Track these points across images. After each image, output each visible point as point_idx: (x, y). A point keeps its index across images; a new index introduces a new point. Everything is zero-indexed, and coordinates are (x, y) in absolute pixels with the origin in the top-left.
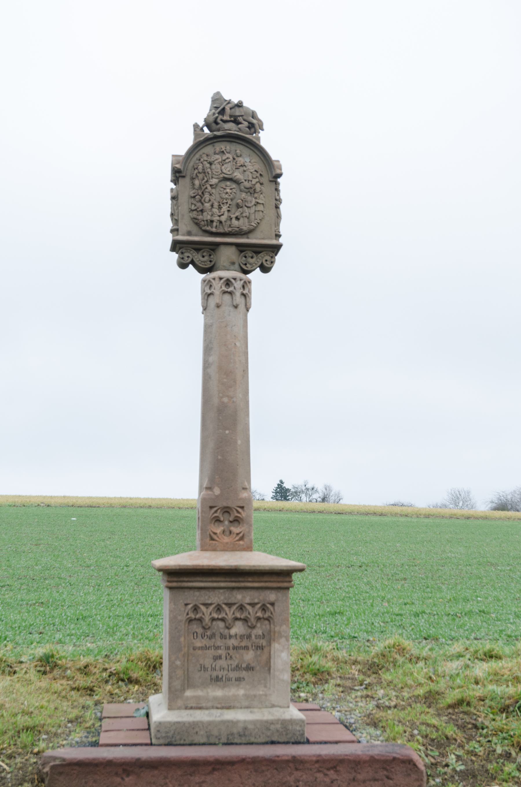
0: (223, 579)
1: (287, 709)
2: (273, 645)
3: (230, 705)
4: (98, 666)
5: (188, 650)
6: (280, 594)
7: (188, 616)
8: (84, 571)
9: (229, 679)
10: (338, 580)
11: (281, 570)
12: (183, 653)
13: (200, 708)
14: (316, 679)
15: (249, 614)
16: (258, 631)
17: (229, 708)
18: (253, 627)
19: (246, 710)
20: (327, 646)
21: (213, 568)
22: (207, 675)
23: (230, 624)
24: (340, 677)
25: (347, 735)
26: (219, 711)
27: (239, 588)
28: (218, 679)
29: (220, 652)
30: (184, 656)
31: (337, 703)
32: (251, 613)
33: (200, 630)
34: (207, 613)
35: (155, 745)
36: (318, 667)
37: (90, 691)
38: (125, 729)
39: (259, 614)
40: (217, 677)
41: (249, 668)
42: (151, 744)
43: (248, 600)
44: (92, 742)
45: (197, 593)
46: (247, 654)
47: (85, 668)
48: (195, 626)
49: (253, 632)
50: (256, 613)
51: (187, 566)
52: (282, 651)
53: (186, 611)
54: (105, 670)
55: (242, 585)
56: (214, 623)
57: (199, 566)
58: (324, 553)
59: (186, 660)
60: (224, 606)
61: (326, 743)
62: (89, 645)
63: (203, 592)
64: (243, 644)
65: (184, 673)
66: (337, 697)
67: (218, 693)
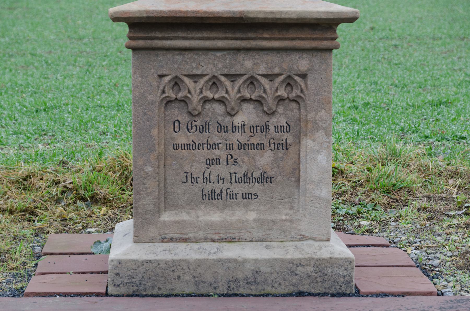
0: (221, 35)
1: (327, 243)
2: (303, 142)
3: (233, 236)
4: (45, 178)
5: (166, 149)
6: (316, 60)
7: (164, 95)
8: (72, 46)
9: (232, 196)
10: (460, 58)
11: (317, 19)
12: (156, 153)
13: (185, 240)
14: (390, 200)
15: (265, 92)
16: (280, 120)
17: (232, 240)
18: (272, 113)
19: (259, 243)
20: (411, 150)
21: (203, 15)
22: (196, 188)
23: (233, 109)
24: (428, 197)
25: (425, 284)
26: (217, 245)
27: (248, 50)
28: (214, 195)
29: (217, 152)
30: (158, 158)
31: (416, 237)
32: (269, 91)
33: (184, 118)
34: (194, 90)
35: (111, 295)
36: (393, 181)
37: (31, 214)
38: (71, 272)
39: (282, 92)
40: (213, 192)
41: (264, 179)
42: (107, 294)
43: (262, 70)
44: (16, 289)
45: (179, 58)
46: (262, 156)
47: (25, 180)
48: (176, 111)
49: (271, 121)
50: (277, 90)
51: (161, 12)
52: (319, 152)
53: (161, 87)
54: (57, 183)
55: (253, 44)
56: (208, 106)
57: (180, 12)
58: (445, 20)
59: (162, 166)
60: (223, 79)
61: (386, 295)
62: (40, 146)
63: (188, 55)
64: (255, 141)
65: (159, 186)
66: (418, 226)
67: (213, 216)
